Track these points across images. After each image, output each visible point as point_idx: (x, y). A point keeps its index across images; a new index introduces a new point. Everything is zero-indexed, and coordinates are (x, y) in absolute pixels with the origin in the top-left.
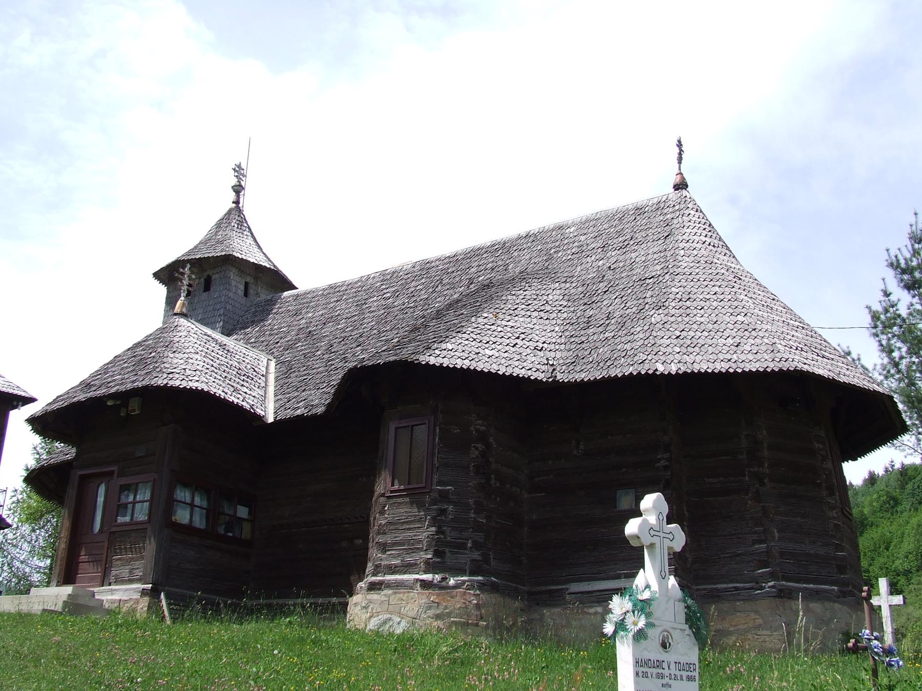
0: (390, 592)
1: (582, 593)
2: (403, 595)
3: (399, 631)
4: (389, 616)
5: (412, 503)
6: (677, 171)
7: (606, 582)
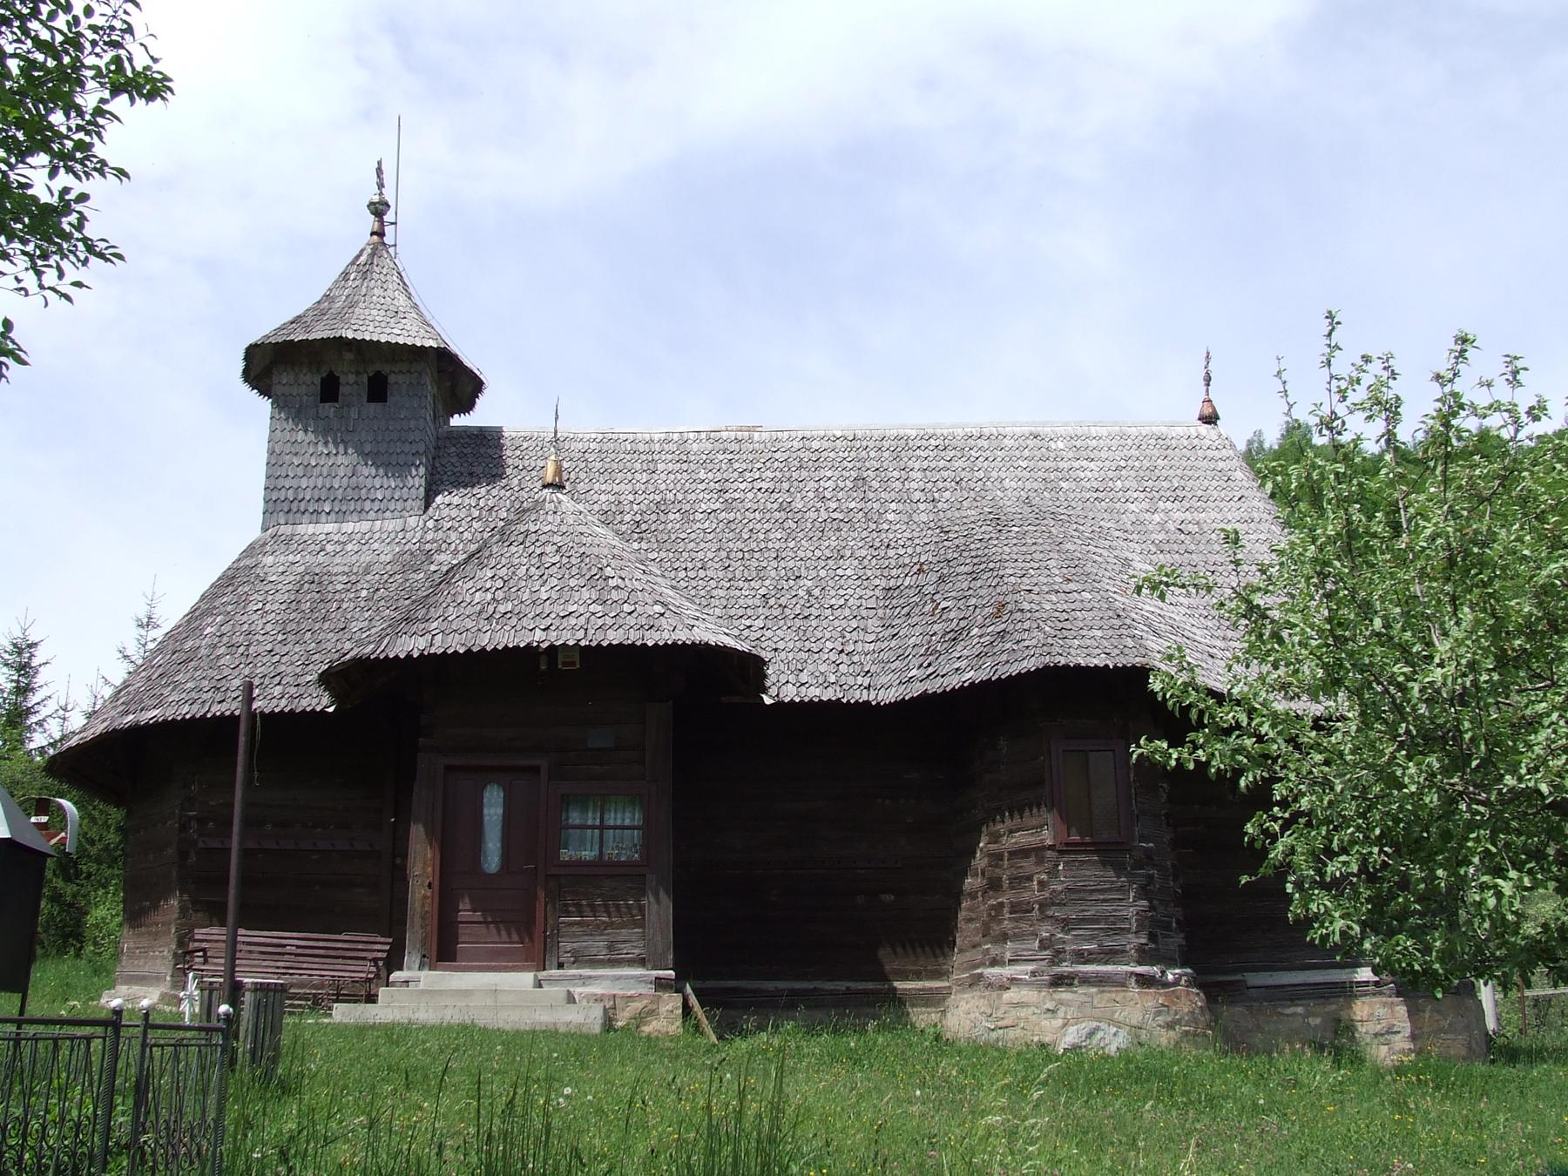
0: (1094, 990)
1: (1276, 987)
2: (1112, 994)
3: (1112, 1049)
4: (1095, 1024)
5: (1104, 864)
6: (1203, 397)
7: (1294, 973)
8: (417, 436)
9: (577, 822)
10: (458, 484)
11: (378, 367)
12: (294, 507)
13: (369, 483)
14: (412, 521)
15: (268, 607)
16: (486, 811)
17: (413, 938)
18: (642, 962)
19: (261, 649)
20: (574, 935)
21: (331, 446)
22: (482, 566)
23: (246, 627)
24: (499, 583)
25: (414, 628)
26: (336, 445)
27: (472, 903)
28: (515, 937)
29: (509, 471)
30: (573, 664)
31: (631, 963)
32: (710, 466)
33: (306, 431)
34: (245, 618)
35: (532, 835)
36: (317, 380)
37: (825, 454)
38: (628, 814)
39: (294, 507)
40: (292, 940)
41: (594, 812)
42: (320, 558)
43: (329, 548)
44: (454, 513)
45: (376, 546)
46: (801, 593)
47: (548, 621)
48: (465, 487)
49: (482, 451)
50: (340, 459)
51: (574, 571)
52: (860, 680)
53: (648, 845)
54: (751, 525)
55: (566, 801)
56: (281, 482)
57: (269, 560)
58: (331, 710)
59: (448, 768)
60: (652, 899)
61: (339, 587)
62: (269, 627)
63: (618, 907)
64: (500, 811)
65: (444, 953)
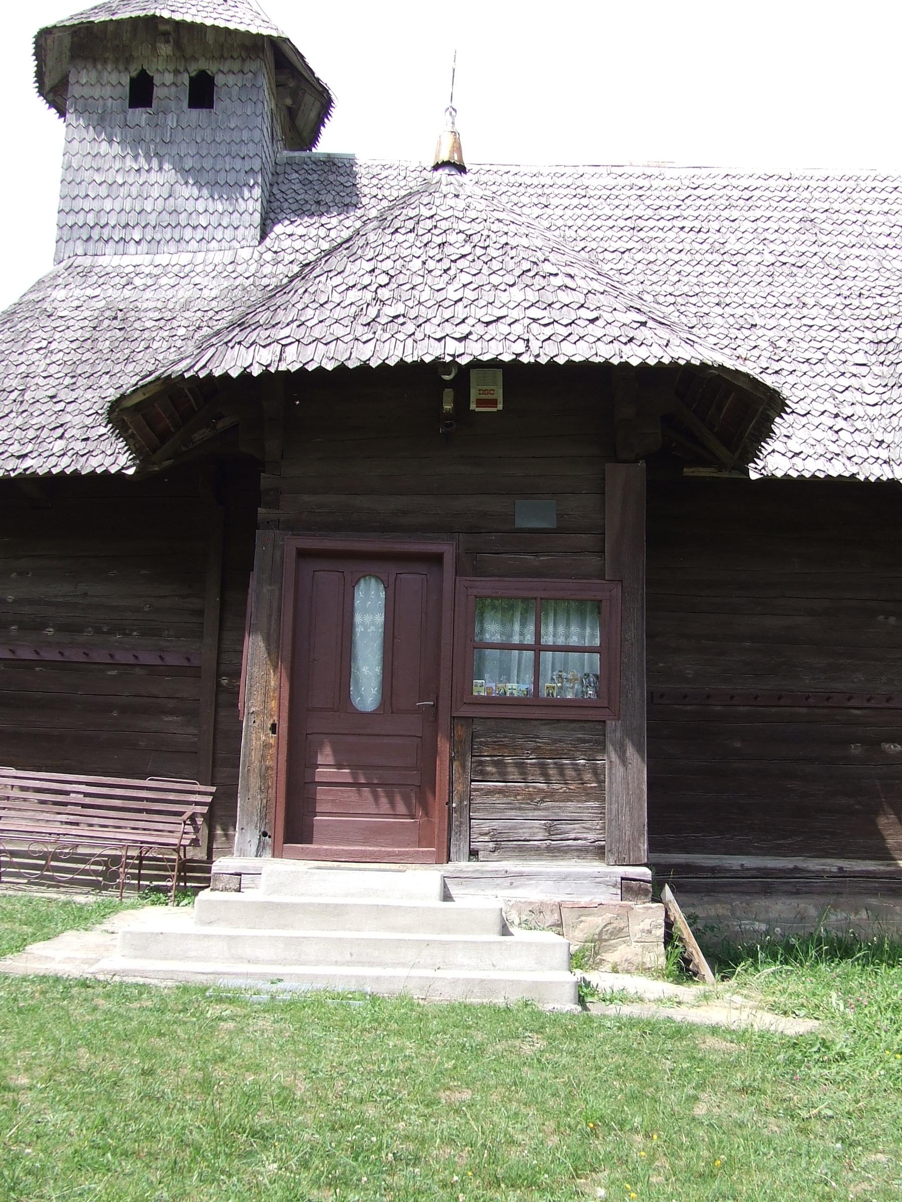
8: (251, 149)
9: (497, 638)
10: (301, 212)
11: (203, 64)
12: (95, 234)
13: (190, 206)
14: (245, 253)
15: (53, 346)
16: (358, 619)
17: (249, 803)
18: (600, 852)
19: (40, 394)
20: (492, 808)
21: (142, 160)
22: (353, 258)
23: (23, 368)
24: (384, 279)
25: (254, 336)
26: (148, 159)
27: (335, 752)
28: (401, 808)
29: (365, 201)
30: (494, 403)
31: (582, 852)
32: (617, 202)
33: (110, 141)
34: (23, 358)
35: (429, 660)
36: (126, 80)
37: (757, 193)
38: (561, 629)
39: (95, 234)
40: (79, 785)
41: (523, 624)
42: (127, 293)
43: (138, 281)
44: (298, 244)
45: (197, 280)
46: (763, 344)
47: (464, 329)
48: (312, 215)
49: (331, 178)
50: (153, 177)
51: (495, 265)
52: (873, 452)
53: (607, 680)
54: (677, 267)
55: (481, 606)
56: (79, 204)
57: (60, 294)
58: (131, 471)
59: (302, 554)
60: (614, 757)
61: (149, 324)
62: (53, 369)
63: (561, 769)
64: (380, 619)
65: (295, 829)
